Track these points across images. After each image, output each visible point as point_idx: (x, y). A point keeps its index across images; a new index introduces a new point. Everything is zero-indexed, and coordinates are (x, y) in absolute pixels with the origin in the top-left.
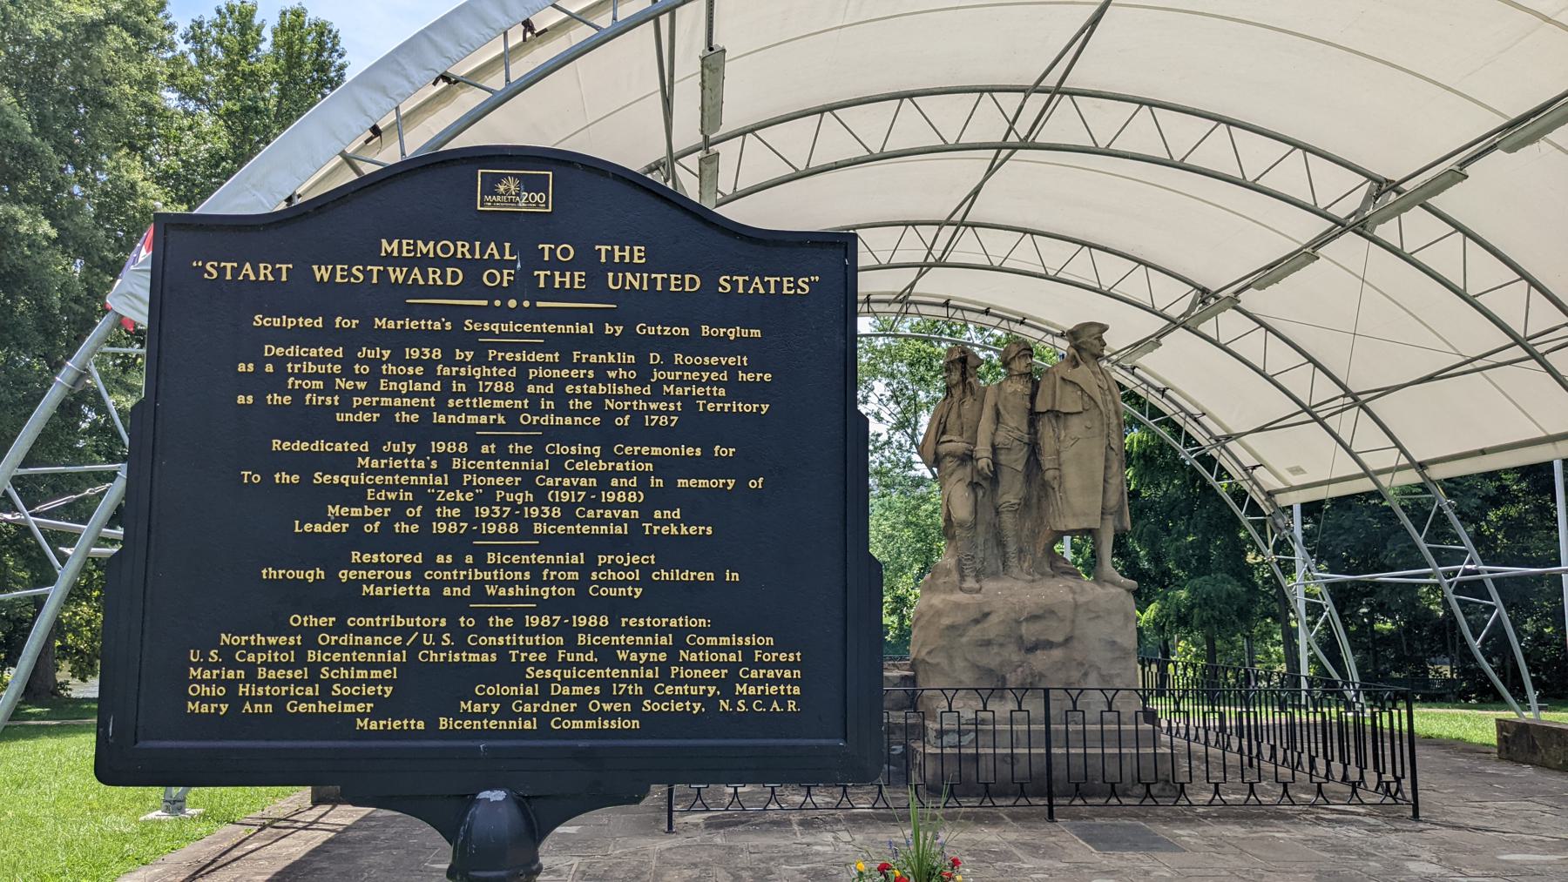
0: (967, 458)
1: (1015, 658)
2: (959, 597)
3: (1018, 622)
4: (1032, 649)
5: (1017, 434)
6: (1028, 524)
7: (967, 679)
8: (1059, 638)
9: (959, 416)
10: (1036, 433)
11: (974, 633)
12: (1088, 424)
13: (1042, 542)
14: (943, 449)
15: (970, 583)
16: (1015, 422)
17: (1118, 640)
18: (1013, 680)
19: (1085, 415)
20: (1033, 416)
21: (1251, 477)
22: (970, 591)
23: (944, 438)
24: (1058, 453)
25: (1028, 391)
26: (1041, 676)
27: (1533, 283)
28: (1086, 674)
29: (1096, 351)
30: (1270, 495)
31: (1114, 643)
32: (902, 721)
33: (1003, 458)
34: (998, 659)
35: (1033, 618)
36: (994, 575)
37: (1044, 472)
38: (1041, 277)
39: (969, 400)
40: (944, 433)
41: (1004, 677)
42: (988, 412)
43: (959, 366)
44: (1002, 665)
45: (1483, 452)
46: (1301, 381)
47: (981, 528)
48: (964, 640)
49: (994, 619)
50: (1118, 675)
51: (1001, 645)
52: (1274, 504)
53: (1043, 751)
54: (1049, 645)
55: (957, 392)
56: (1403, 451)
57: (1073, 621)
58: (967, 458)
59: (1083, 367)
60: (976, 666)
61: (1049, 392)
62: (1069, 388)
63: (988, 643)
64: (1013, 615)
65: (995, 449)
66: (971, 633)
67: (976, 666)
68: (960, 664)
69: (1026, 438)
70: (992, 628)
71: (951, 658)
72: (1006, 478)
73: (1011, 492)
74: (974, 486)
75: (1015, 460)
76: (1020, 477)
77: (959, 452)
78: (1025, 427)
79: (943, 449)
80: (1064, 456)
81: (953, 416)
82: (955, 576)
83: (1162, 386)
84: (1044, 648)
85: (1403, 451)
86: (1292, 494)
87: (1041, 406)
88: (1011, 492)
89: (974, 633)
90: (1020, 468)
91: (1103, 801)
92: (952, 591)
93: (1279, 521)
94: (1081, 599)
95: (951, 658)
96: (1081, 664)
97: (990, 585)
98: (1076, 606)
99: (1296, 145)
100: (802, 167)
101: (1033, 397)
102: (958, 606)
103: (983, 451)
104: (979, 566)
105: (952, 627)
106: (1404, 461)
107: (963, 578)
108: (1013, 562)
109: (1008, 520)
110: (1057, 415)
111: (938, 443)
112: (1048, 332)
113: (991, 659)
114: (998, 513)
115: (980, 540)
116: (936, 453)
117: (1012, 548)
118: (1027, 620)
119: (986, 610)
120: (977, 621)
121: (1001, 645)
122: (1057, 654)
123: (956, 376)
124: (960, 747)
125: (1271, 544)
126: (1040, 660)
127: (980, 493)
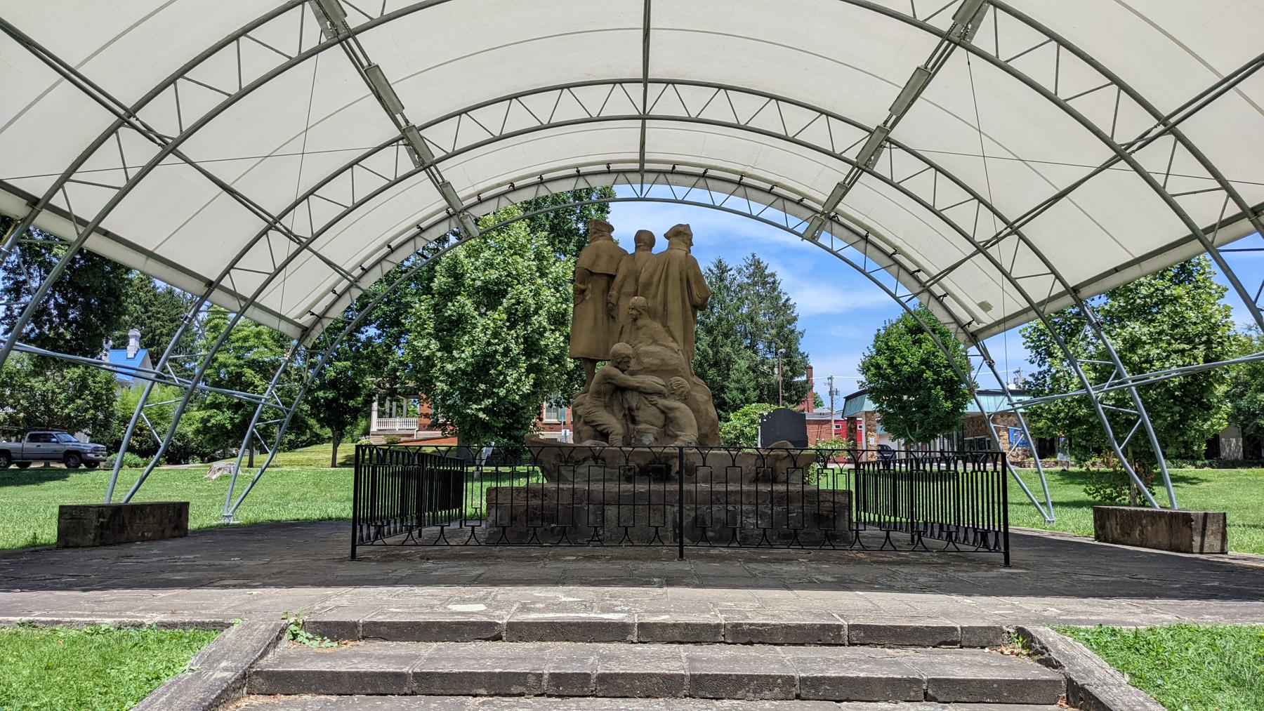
27: (1123, 87)
45: (1116, 270)
46: (965, 214)
56: (1232, 194)
85: (1058, 277)
106: (1233, 209)
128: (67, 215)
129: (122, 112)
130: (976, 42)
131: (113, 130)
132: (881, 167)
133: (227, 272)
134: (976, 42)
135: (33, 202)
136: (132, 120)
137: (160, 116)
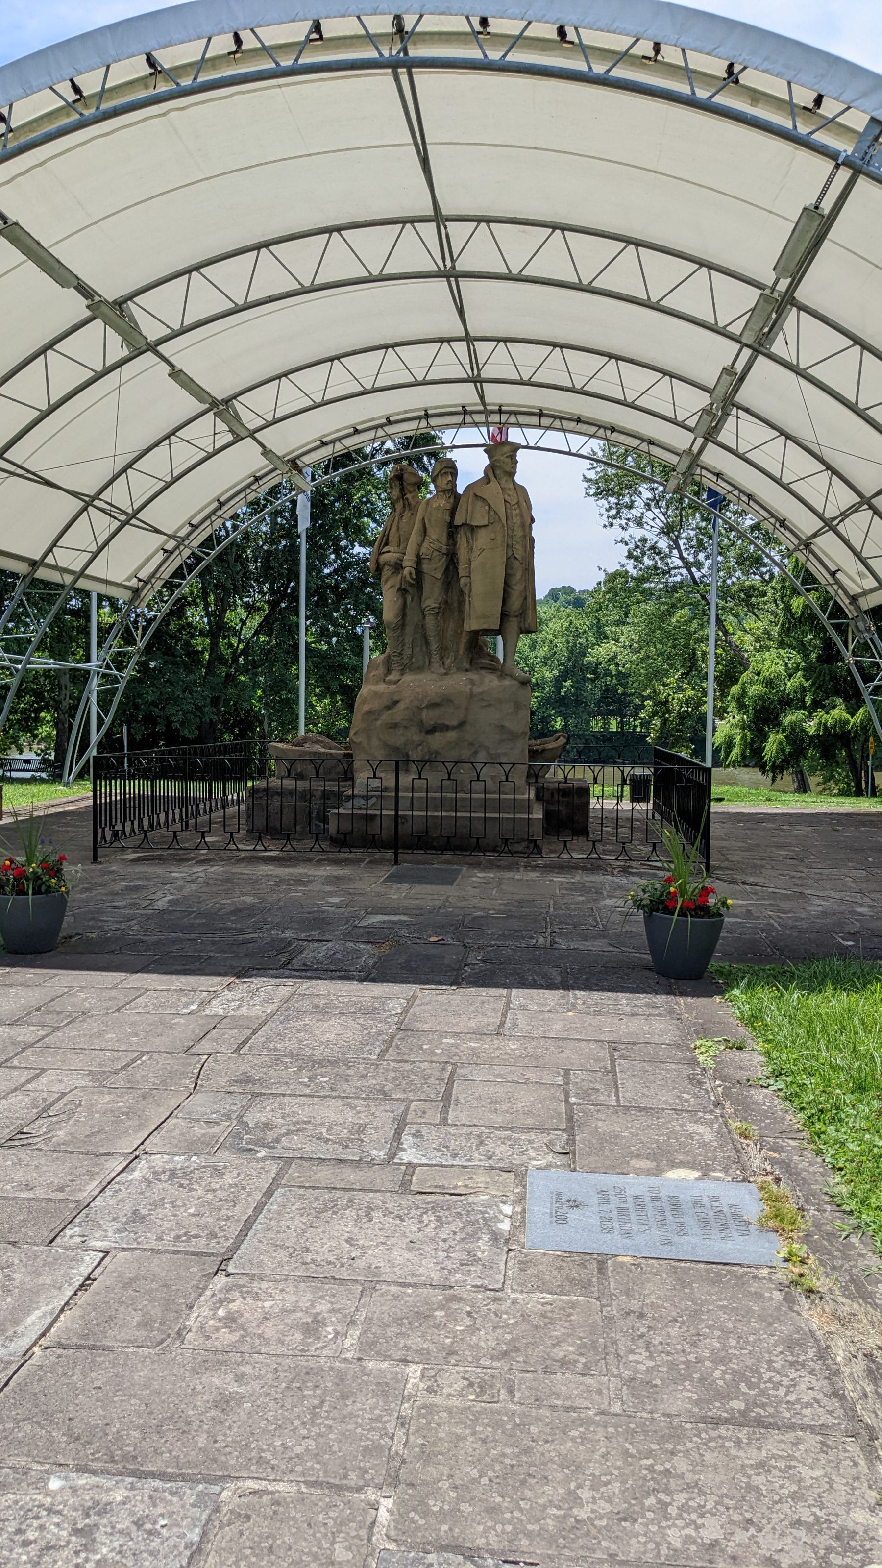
0: (398, 567)
1: (417, 738)
2: (381, 687)
3: (420, 709)
4: (432, 730)
5: (436, 545)
6: (452, 625)
7: (380, 754)
8: (455, 723)
9: (398, 529)
10: (455, 544)
11: (386, 717)
12: (493, 536)
13: (464, 640)
14: (384, 558)
15: (392, 677)
16: (437, 534)
17: (507, 724)
18: (414, 755)
19: (490, 527)
20: (452, 530)
21: (837, 582)
22: (391, 682)
23: (386, 549)
24: (470, 562)
25: (449, 506)
26: (437, 753)
28: (476, 753)
29: (507, 469)
30: (854, 599)
31: (502, 726)
32: (336, 789)
33: (425, 567)
34: (403, 739)
35: (433, 705)
36: (420, 669)
37: (458, 579)
38: (568, 390)
39: (407, 514)
40: (386, 544)
41: (407, 754)
42: (417, 525)
43: (398, 483)
44: (405, 744)
47: (409, 629)
48: (379, 723)
49: (401, 706)
50: (505, 754)
51: (406, 727)
52: (858, 608)
53: (393, 813)
54: (446, 728)
55: (399, 506)
57: (467, 709)
58: (398, 567)
59: (494, 483)
60: (385, 745)
61: (464, 507)
62: (479, 503)
63: (395, 726)
64: (416, 703)
65: (419, 560)
66: (384, 717)
67: (385, 745)
68: (375, 742)
69: (444, 549)
70: (398, 713)
71: (369, 738)
72: (427, 585)
73: (432, 598)
74: (402, 591)
75: (434, 570)
76: (439, 584)
77: (392, 561)
78: (444, 539)
79: (384, 558)
80: (474, 565)
81: (394, 528)
82: (381, 670)
83: (216, 504)
84: (441, 730)
86: (869, 597)
87: (458, 521)
88: (432, 598)
89: (386, 717)
90: (438, 576)
91: (252, 847)
92: (377, 683)
93: (861, 625)
94: (477, 690)
95: (369, 738)
96: (472, 744)
97: (408, 678)
98: (472, 695)
99: (188, 271)
100: (307, 284)
101: (453, 512)
102: (376, 695)
103: (409, 562)
104: (406, 661)
105: (369, 713)
107: (389, 671)
108: (435, 658)
109: (430, 622)
110: (473, 529)
111: (380, 553)
112: (643, 440)
113: (398, 739)
114: (424, 616)
115: (408, 640)
116: (377, 562)
117: (434, 646)
118: (427, 707)
119: (396, 698)
120: (388, 708)
121: (406, 727)
122: (452, 735)
123: (396, 493)
124: (367, 809)
125: (851, 647)
126: (437, 741)
127: (409, 599)
128: (55, 568)
129: (87, 499)
130: (721, 438)
131: (85, 509)
132: (726, 436)
133: (50, 550)
134: (721, 438)
135: (34, 564)
136: (96, 503)
137: (118, 495)
